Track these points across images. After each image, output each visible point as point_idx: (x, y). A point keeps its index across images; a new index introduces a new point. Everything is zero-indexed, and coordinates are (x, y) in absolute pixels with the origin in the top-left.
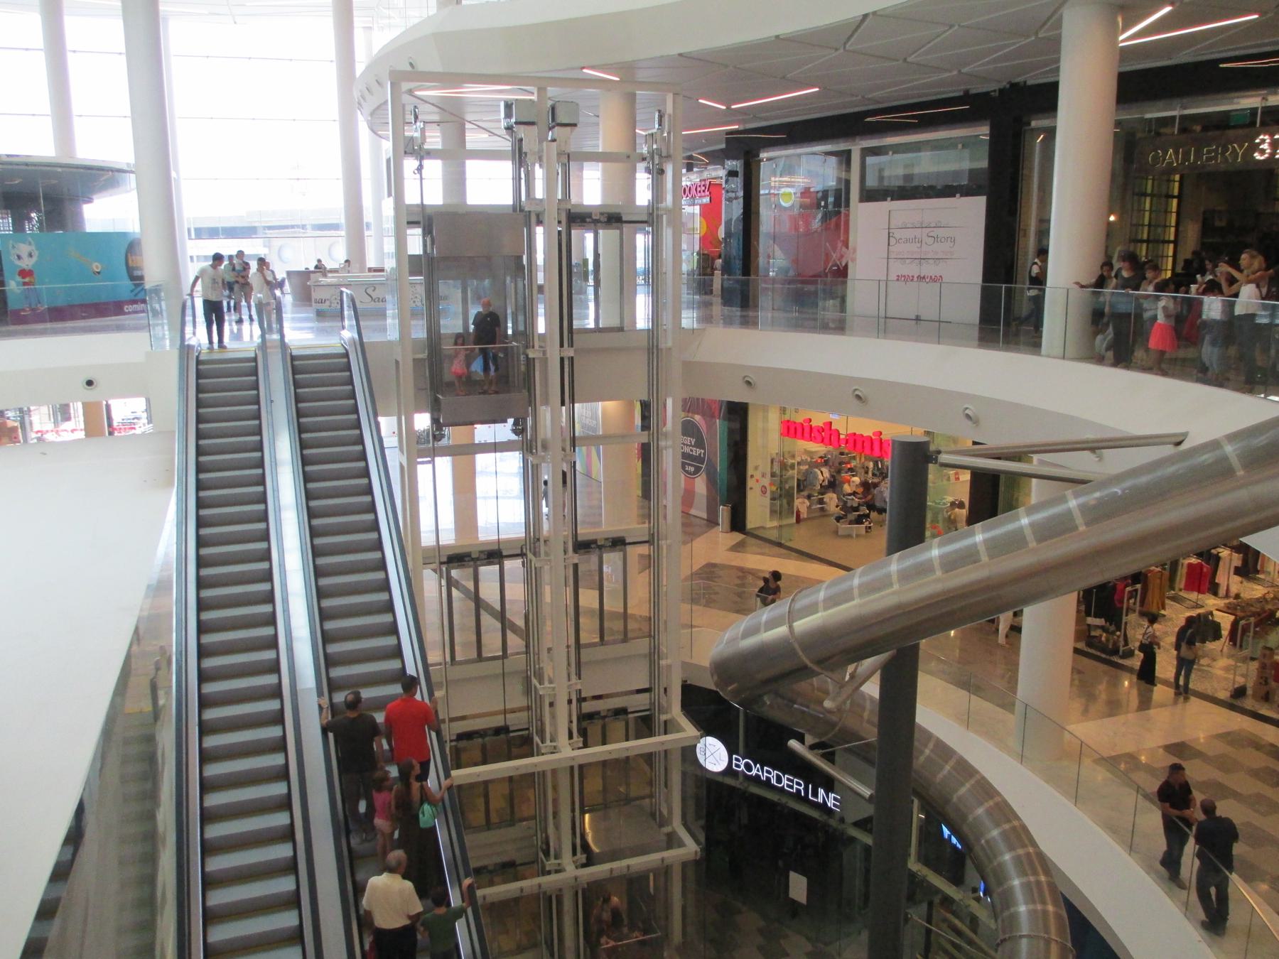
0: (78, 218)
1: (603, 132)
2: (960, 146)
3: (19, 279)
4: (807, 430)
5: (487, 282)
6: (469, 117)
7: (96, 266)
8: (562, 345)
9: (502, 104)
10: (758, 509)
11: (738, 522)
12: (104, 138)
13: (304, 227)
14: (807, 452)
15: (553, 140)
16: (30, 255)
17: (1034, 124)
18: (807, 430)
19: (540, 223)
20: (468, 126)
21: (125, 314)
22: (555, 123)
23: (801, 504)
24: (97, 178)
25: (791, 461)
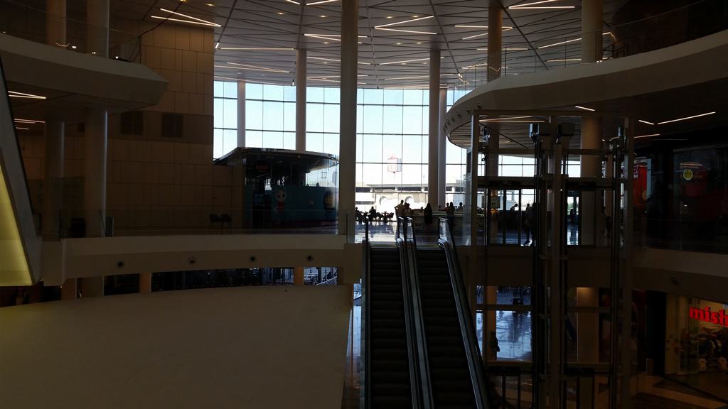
0: (304, 178)
1: (587, 138)
2: (453, 190)
3: (277, 206)
4: (707, 314)
5: (359, 238)
6: (502, 132)
7: (311, 203)
8: (561, 253)
9: (531, 125)
10: (672, 363)
11: (659, 369)
12: (324, 141)
13: (393, 188)
14: (705, 329)
15: (559, 143)
16: (284, 196)
17: (674, 151)
18: (707, 314)
19: (550, 187)
20: (501, 137)
21: (320, 226)
22: (561, 134)
23: (702, 363)
24: (318, 160)
25: (693, 336)
